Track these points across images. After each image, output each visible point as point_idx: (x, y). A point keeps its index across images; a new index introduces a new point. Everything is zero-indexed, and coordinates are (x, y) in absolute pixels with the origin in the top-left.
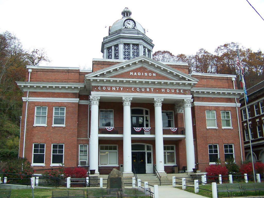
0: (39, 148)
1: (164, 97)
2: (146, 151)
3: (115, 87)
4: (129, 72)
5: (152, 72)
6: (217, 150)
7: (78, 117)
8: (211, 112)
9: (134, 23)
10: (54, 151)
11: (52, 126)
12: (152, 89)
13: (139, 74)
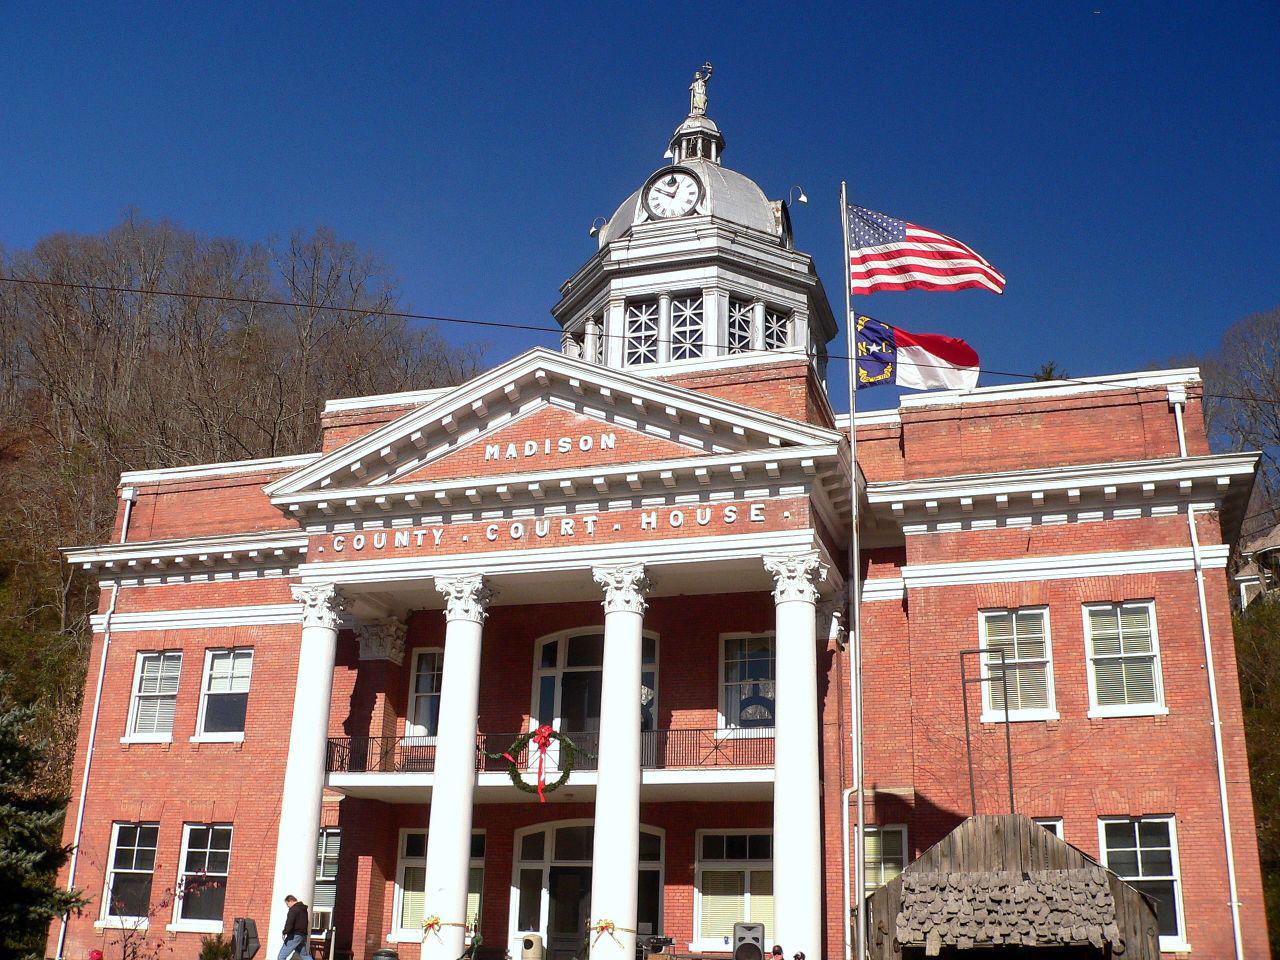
0: (138, 838)
1: (644, 560)
4: (479, 448)
6: (1169, 852)
8: (1020, 618)
9: (695, 188)
13: (530, 447)
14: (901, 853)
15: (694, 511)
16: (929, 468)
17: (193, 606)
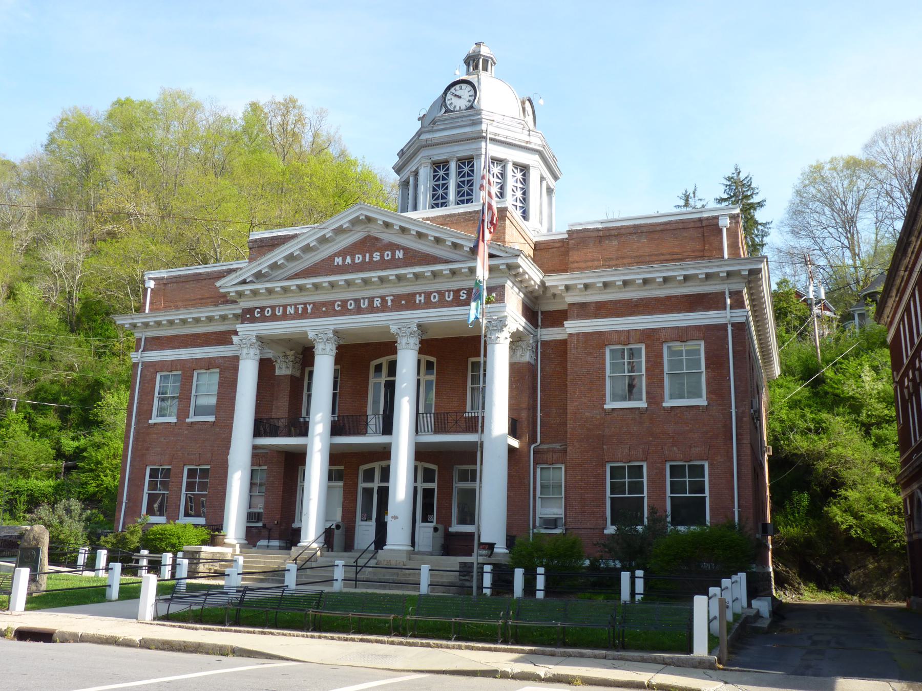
4: (331, 258)
5: (393, 247)
10: (190, 486)
11: (606, 407)
12: (389, 299)
13: (358, 258)
14: (303, 430)
15: (444, 294)
16: (583, 265)
17: (186, 347)
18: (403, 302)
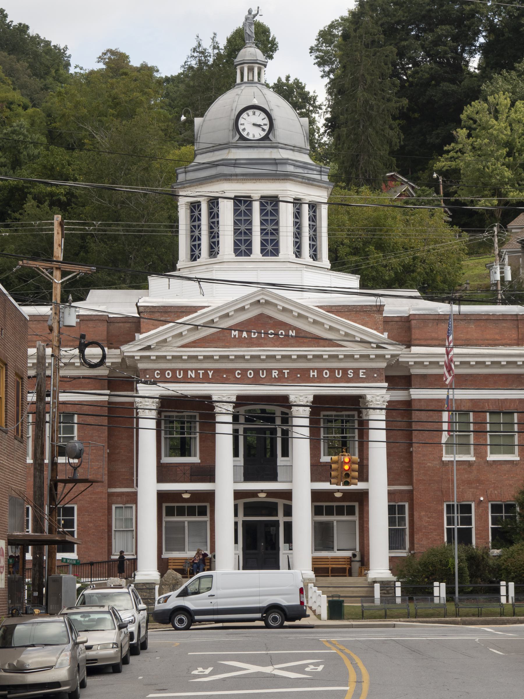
2: (281, 518)
3: (194, 371)
7: (108, 438)
18: (299, 376)
